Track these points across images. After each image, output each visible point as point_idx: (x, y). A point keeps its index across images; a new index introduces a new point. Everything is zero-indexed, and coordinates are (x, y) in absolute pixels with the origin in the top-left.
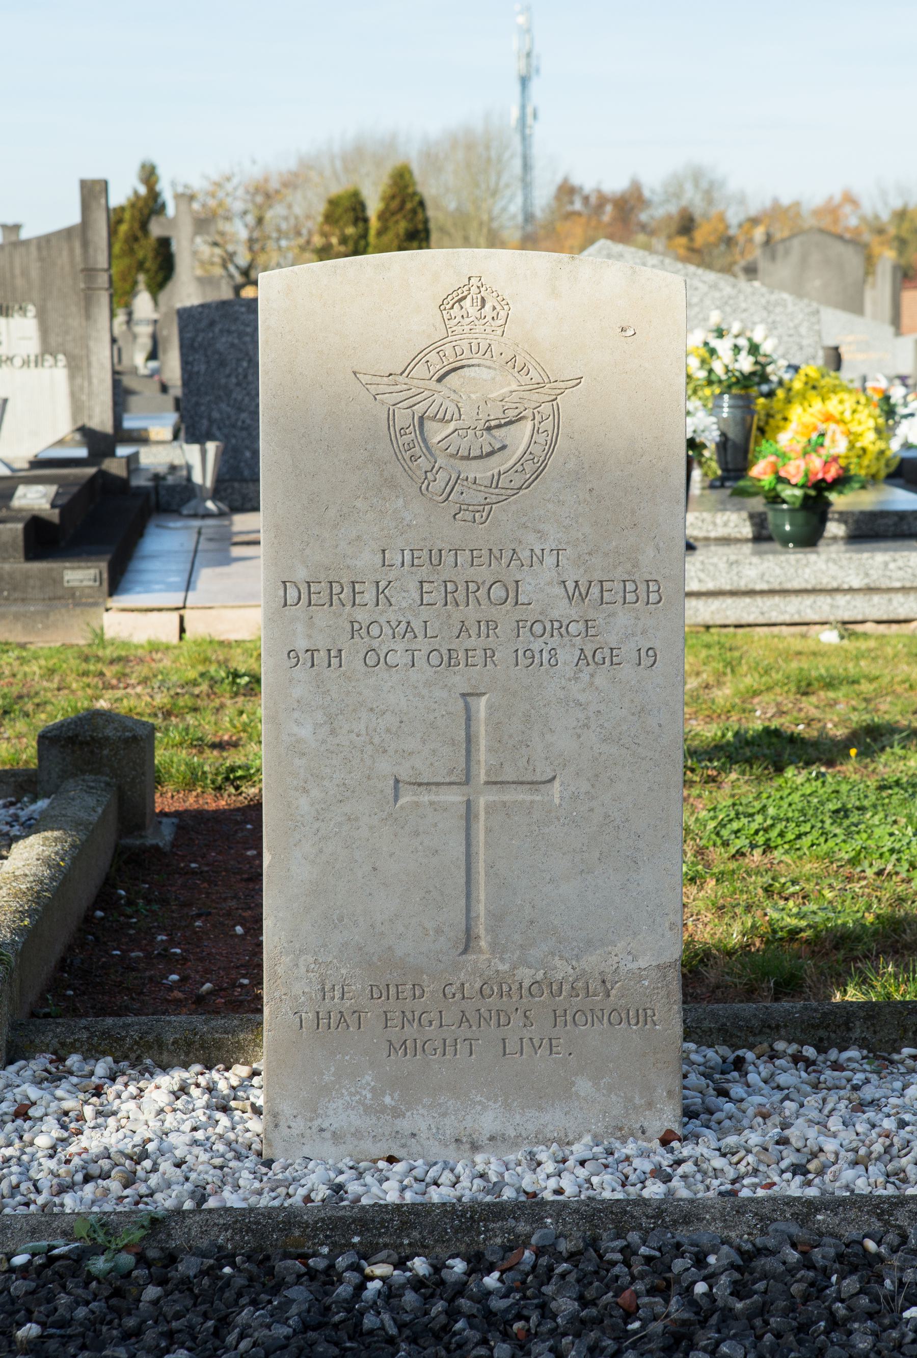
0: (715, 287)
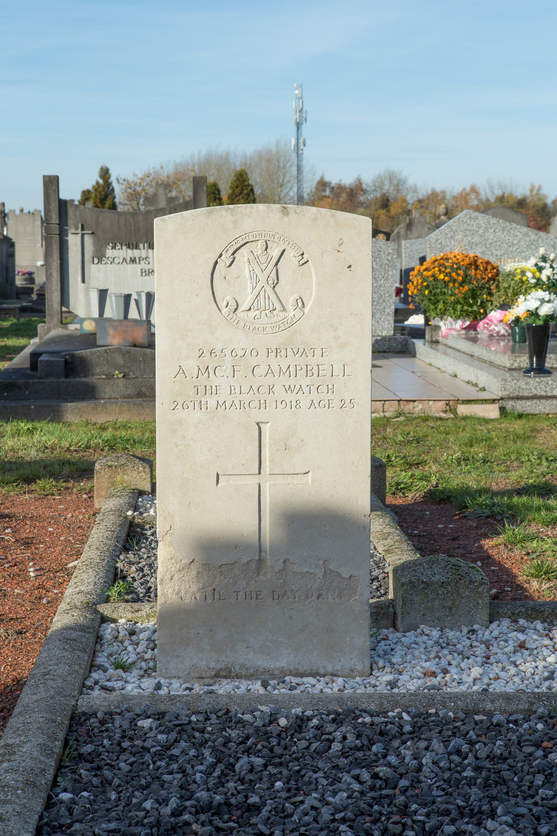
0: (526, 235)
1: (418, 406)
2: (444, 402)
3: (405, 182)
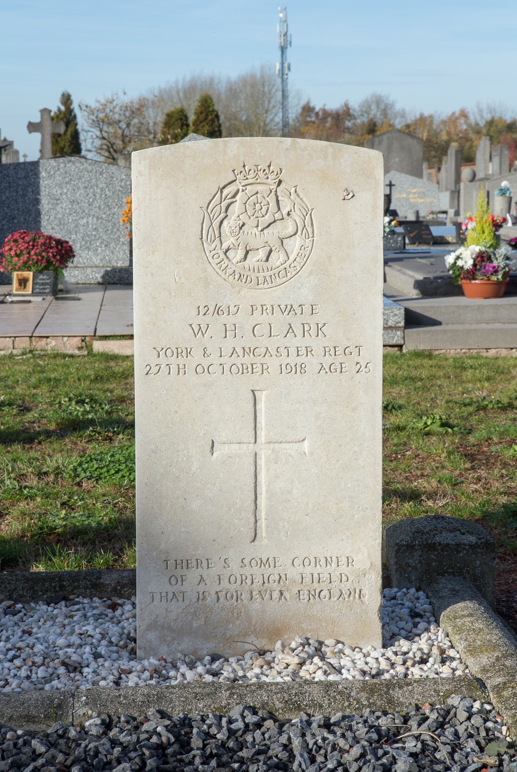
1: (51, 343)
2: (79, 338)
3: (393, 105)
